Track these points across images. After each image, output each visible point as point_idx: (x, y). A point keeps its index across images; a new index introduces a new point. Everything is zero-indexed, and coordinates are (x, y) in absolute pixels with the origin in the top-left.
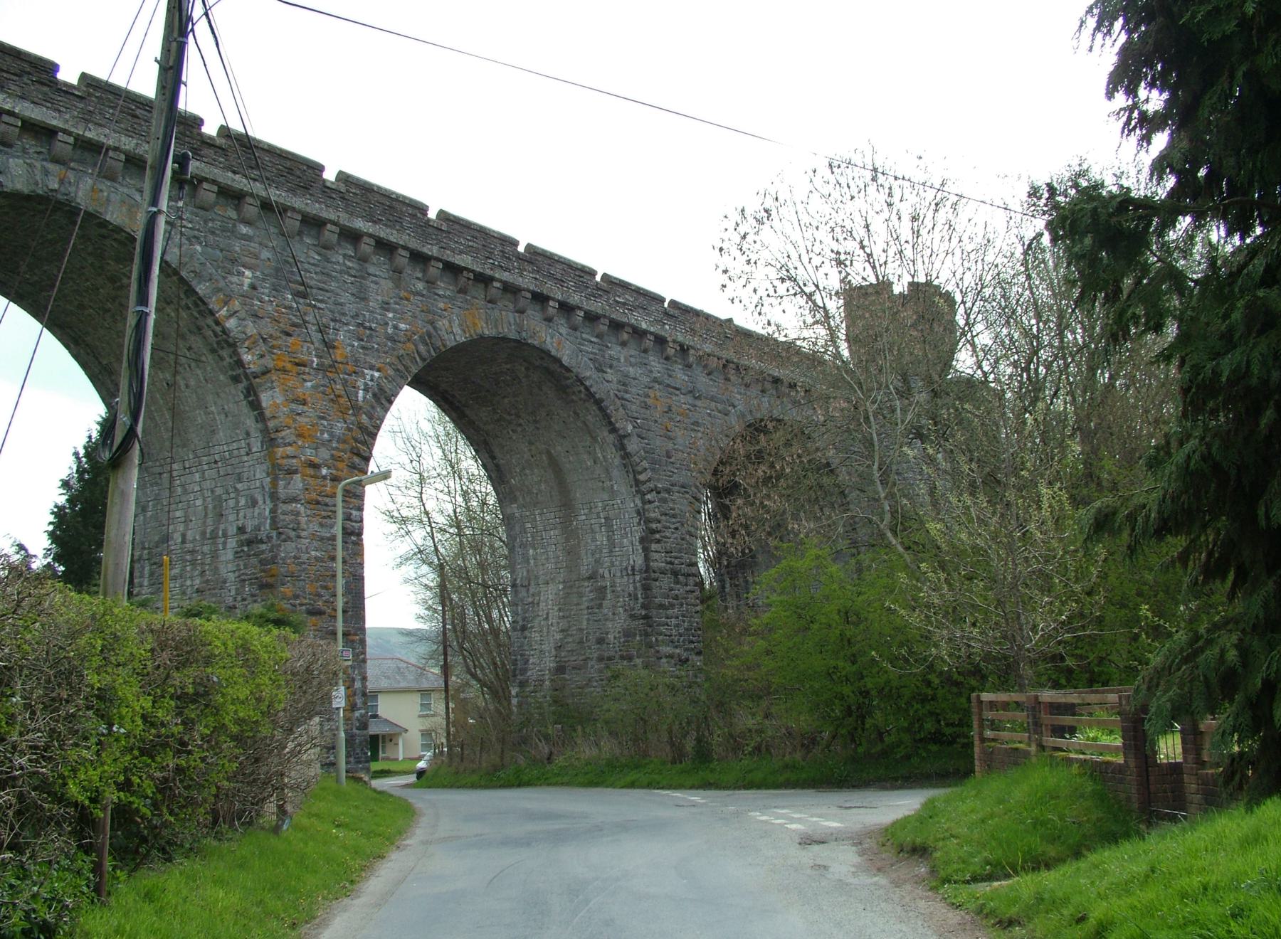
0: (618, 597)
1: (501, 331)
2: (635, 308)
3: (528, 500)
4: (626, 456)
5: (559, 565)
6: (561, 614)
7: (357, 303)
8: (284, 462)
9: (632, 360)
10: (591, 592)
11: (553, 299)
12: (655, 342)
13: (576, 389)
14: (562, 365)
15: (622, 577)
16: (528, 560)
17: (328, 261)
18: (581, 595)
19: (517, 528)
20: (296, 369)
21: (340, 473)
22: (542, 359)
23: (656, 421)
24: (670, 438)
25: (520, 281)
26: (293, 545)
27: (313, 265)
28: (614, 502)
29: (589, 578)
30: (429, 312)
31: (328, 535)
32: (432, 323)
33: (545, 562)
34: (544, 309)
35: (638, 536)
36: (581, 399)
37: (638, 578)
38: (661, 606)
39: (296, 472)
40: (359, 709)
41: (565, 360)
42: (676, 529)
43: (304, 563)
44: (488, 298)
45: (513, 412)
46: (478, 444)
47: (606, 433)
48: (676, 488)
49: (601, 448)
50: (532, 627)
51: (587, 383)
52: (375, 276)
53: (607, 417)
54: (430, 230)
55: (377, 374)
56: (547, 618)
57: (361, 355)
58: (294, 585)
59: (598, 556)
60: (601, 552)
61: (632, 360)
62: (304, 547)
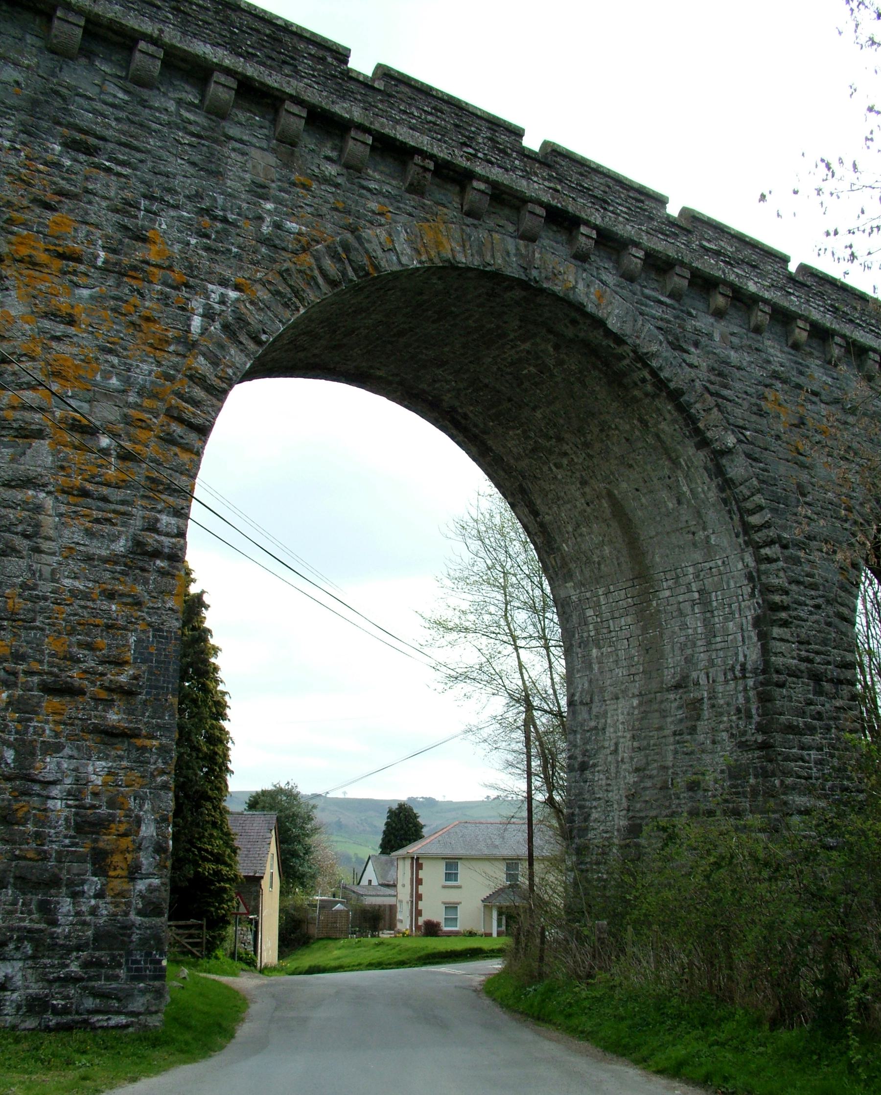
0: (721, 714)
1: (488, 259)
2: (740, 263)
3: (587, 573)
4: (727, 484)
5: (633, 671)
6: (636, 744)
7: (201, 178)
8: (11, 414)
9: (735, 340)
10: (679, 708)
11: (587, 223)
12: (772, 317)
13: (636, 376)
14: (609, 333)
15: (726, 682)
16: (591, 664)
17: (144, 103)
18: (664, 714)
19: (575, 619)
20: (58, 264)
21: (139, 447)
22: (574, 322)
23: (778, 437)
24: (803, 466)
25: (522, 185)
26: (23, 563)
27: (113, 106)
28: (712, 564)
29: (677, 687)
30: (349, 213)
31: (104, 553)
32: (353, 230)
33: (613, 666)
34: (571, 239)
35: (750, 614)
36: (647, 395)
37: (751, 683)
38: (791, 729)
39: (39, 434)
40: (148, 876)
41: (613, 324)
42: (818, 607)
43: (45, 599)
44: (465, 208)
45: (551, 433)
46: (513, 495)
47: (691, 451)
48: (814, 544)
49: (687, 477)
50: (594, 765)
51: (654, 364)
52: (241, 141)
53: (691, 420)
54: (352, 86)
55: (233, 294)
56: (616, 751)
57: (203, 259)
58: (15, 635)
59: (689, 652)
60: (694, 645)
61: (735, 340)
62: (47, 571)
